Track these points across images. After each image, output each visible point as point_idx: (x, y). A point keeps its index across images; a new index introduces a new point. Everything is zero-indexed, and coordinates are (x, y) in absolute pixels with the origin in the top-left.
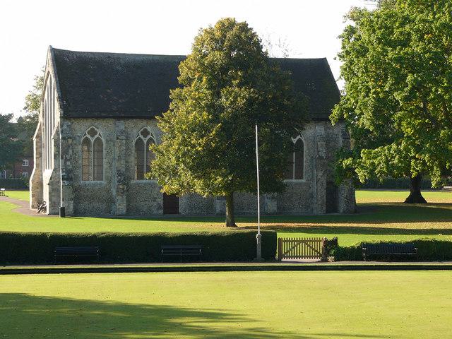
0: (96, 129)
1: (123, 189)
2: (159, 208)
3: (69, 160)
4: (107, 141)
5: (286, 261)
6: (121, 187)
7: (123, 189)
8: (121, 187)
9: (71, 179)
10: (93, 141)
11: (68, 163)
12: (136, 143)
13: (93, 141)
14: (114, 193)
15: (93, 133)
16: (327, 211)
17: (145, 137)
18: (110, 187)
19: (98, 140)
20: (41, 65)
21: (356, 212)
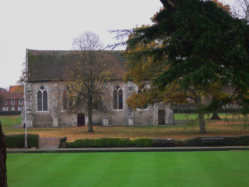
0: (44, 87)
1: (56, 115)
2: (75, 123)
3: (30, 101)
4: (49, 92)
5: (41, 149)
6: (55, 114)
7: (56, 115)
8: (55, 114)
9: (31, 110)
10: (42, 92)
11: (30, 103)
12: (38, 92)
13: (42, 92)
14: (53, 117)
15: (42, 88)
16: (159, 124)
17: (42, 90)
18: (51, 114)
19: (45, 92)
20: (23, 58)
21: (174, 124)
